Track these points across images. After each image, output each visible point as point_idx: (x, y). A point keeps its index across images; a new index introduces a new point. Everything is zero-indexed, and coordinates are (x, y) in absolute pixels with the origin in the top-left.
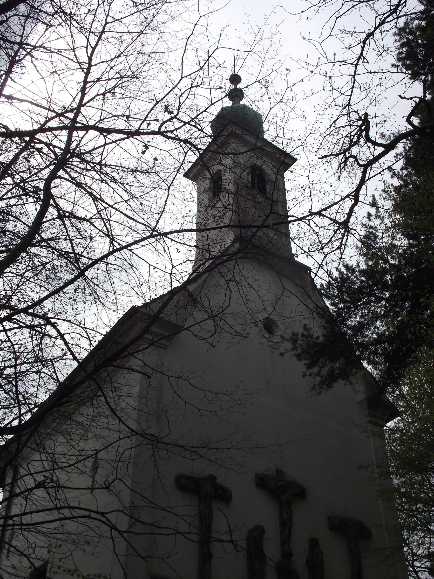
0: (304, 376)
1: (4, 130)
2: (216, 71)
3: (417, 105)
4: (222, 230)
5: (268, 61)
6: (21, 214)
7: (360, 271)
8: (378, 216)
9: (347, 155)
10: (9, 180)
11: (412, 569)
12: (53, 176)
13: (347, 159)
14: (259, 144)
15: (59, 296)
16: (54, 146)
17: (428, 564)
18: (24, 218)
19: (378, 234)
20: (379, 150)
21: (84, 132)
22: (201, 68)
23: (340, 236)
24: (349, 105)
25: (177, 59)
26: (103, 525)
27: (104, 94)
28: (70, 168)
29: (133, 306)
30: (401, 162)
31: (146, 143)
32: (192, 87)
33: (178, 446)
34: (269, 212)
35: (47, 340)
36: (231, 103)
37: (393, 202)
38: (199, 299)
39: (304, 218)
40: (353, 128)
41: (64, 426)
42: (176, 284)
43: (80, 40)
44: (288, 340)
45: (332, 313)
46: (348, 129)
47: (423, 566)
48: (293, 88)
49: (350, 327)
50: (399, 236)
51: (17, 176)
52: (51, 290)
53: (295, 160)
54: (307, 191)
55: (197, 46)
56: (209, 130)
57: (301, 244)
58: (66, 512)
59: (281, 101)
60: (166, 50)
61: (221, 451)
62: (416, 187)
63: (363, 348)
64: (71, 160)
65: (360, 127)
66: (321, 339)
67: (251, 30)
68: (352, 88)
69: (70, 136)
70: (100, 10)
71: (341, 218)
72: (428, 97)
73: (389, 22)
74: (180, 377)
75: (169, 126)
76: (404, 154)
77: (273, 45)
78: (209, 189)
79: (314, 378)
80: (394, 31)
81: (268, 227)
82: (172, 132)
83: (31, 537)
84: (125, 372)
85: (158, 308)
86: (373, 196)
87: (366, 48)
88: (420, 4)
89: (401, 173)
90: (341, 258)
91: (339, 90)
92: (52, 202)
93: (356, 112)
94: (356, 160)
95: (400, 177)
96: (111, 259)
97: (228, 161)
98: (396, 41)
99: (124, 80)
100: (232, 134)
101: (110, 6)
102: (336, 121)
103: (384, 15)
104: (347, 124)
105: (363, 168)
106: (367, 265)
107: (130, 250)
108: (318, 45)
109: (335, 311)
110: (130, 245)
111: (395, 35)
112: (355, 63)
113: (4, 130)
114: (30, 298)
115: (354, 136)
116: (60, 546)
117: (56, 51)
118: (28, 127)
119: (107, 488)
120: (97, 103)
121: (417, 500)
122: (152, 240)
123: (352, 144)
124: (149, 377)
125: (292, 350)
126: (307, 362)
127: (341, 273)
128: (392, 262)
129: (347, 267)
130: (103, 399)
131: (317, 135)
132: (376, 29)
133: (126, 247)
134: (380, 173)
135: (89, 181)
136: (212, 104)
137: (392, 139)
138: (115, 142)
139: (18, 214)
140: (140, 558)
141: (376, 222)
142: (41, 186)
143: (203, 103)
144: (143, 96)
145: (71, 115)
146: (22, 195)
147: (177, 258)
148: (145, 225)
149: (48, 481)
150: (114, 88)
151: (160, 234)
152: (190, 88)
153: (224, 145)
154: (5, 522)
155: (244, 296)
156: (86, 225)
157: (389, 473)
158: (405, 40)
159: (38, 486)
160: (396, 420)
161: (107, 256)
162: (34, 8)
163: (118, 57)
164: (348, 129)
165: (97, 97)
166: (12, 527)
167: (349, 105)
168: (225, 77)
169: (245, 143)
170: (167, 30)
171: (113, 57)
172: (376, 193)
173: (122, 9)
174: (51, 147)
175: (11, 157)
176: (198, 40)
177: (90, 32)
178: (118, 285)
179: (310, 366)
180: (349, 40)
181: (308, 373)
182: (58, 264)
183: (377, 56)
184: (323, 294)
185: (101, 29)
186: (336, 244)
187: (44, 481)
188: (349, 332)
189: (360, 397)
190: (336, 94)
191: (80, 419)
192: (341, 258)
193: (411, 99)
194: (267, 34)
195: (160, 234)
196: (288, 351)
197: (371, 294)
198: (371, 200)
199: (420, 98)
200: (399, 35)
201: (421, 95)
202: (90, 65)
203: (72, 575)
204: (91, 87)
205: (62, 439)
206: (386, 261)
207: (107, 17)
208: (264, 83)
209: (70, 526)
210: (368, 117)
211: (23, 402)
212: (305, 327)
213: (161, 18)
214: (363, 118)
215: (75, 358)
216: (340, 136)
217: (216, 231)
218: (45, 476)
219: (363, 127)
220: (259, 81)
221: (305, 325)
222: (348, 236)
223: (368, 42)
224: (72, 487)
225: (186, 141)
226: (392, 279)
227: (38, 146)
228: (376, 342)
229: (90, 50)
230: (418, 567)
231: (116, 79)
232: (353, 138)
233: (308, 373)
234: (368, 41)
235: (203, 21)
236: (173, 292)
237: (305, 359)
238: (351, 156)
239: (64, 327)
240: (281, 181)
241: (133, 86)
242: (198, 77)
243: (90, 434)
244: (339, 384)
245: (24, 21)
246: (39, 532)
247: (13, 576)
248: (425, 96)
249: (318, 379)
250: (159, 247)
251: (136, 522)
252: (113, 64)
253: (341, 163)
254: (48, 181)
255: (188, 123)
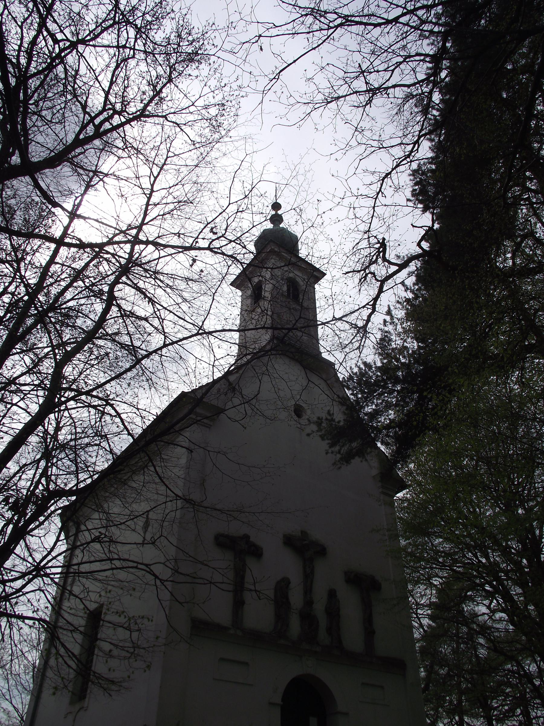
0: (327, 453)
1: (78, 242)
2: (259, 199)
3: (427, 232)
4: (259, 331)
5: (302, 193)
6: (90, 312)
7: (376, 367)
8: (392, 323)
9: (367, 271)
10: (80, 283)
11: (415, 616)
12: (117, 282)
13: (367, 275)
14: (293, 260)
15: (120, 381)
16: (120, 257)
17: (429, 612)
18: (92, 316)
19: (392, 337)
20: (394, 268)
21: (145, 246)
22: (246, 196)
23: (359, 338)
24: (369, 231)
25: (226, 188)
26: (147, 574)
27: (163, 215)
28: (133, 275)
29: (183, 392)
30: (413, 279)
31: (195, 258)
32: (238, 212)
33: (216, 509)
34: (298, 317)
35: (108, 418)
36: (272, 225)
37: (405, 311)
38: (237, 387)
39: (328, 323)
40: (372, 249)
41: (121, 491)
42: (218, 375)
43: (144, 170)
44: (314, 423)
45: (352, 400)
46: (368, 250)
47: (425, 613)
48: (323, 215)
49: (366, 414)
50: (409, 340)
51: (87, 280)
52: (113, 376)
53: (325, 274)
54: (330, 301)
55: (243, 179)
56: (252, 247)
57: (325, 344)
58: (118, 563)
59: (312, 226)
60: (217, 181)
61: (253, 514)
62: (425, 300)
63: (377, 432)
64: (133, 268)
65: (379, 249)
66: (342, 424)
67: (288, 167)
68: (372, 217)
69: (132, 249)
70: (162, 147)
71: (360, 324)
72: (436, 226)
73: (403, 165)
74: (219, 452)
75: (216, 244)
76: (416, 272)
77: (307, 180)
78: (251, 296)
79: (336, 455)
80: (409, 172)
81: (296, 329)
82: (219, 248)
83: (88, 583)
84: (172, 446)
85: (201, 394)
86: (389, 306)
87: (384, 184)
88: (430, 151)
89: (412, 288)
90: (359, 357)
91: (361, 218)
92: (114, 302)
93: (375, 237)
94: (375, 276)
95: (412, 291)
96: (164, 350)
97: (268, 275)
98: (411, 180)
99: (181, 204)
100: (272, 252)
101: (171, 144)
102: (358, 243)
103: (399, 159)
104: (367, 246)
105: (379, 283)
106: (382, 363)
107: (180, 345)
108: (344, 181)
109: (354, 400)
110: (181, 340)
111: (410, 175)
112: (375, 197)
113: (78, 242)
114: (95, 382)
115: (373, 256)
116: (110, 591)
117: (126, 178)
118: (99, 241)
119: (153, 543)
120: (157, 222)
121: (422, 558)
122: (199, 337)
123: (371, 263)
124: (192, 451)
125: (317, 431)
126: (330, 441)
127: (360, 369)
128: (403, 361)
129: (365, 363)
130: (152, 469)
131: (341, 256)
132: (393, 169)
133: (176, 342)
134: (392, 287)
135: (148, 286)
136: (253, 227)
137: (405, 259)
138: (171, 255)
139: (87, 312)
140: (177, 603)
141: (390, 328)
142: (106, 289)
143: (246, 225)
144: (197, 218)
145: (134, 232)
146: (92, 296)
147: (219, 353)
148: (193, 325)
149: (103, 536)
150: (172, 210)
151: (205, 333)
152: (236, 213)
153: (263, 261)
154: (68, 570)
155: (276, 386)
156: (143, 323)
157: (397, 536)
158: (418, 180)
159: (93, 541)
160: (404, 492)
161: (161, 349)
162: (108, 143)
163: (176, 185)
164: (368, 250)
165: (158, 218)
166: (73, 575)
167: (369, 231)
168: (266, 205)
169: (281, 258)
170: (218, 165)
171: (171, 185)
172: (390, 304)
173: (182, 146)
174: (117, 257)
175: (83, 265)
176: (243, 173)
177: (154, 163)
178: (170, 374)
179: (332, 445)
180: (371, 178)
181: (330, 451)
182: (120, 354)
183: (394, 192)
184: (344, 386)
185: (163, 161)
186: (357, 344)
187: (99, 537)
188: (366, 417)
189: (375, 472)
190: (359, 221)
191: (134, 485)
192: (359, 357)
193: (421, 227)
194: (302, 171)
195: (205, 333)
196: (314, 432)
197: (385, 387)
198: (386, 309)
199: (429, 227)
200: (413, 175)
201: (430, 224)
202: (152, 191)
203: (120, 616)
204: (152, 209)
205: (118, 502)
206: (398, 360)
207: (168, 152)
208: (298, 211)
209: (122, 575)
210: (386, 241)
211: (86, 469)
212: (329, 412)
213: (213, 154)
214: (381, 241)
215: (129, 434)
216: (361, 256)
217: (253, 332)
218: (100, 532)
219: (381, 249)
220: (294, 209)
221: (329, 412)
222: (365, 339)
223: (386, 180)
224: (126, 542)
225: (231, 256)
226: (403, 375)
227: (106, 256)
228: (388, 427)
229: (152, 179)
230: (420, 614)
231: (173, 203)
232: (372, 258)
233: (330, 451)
234: (386, 179)
235: (248, 159)
236: (215, 382)
237: (328, 439)
238: (370, 273)
239: (121, 408)
240: (312, 291)
241: (187, 209)
242: (243, 204)
243: (142, 497)
244: (357, 460)
245: (99, 153)
246: (96, 579)
247: (72, 616)
248: (433, 226)
249: (339, 456)
250: (205, 342)
251: (176, 573)
252: (171, 191)
253: (362, 278)
254: (112, 286)
255: (234, 241)
